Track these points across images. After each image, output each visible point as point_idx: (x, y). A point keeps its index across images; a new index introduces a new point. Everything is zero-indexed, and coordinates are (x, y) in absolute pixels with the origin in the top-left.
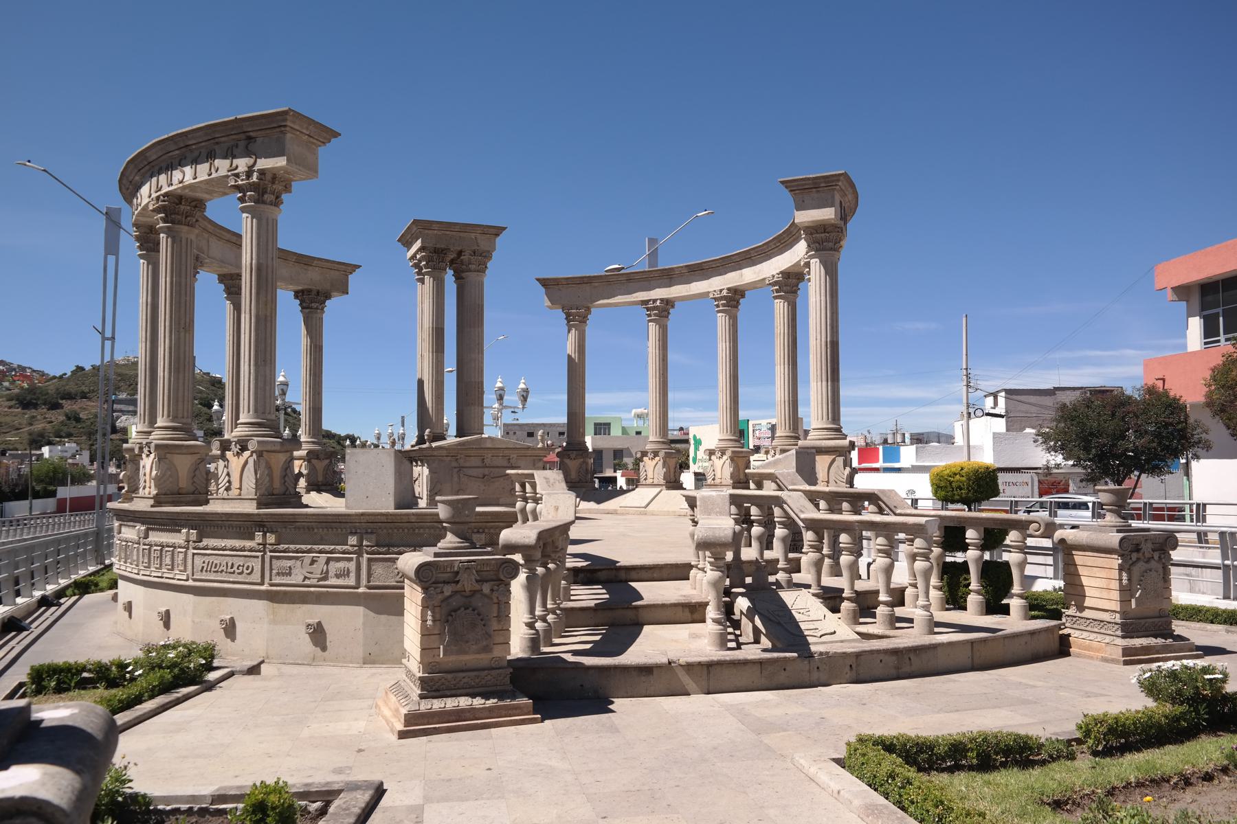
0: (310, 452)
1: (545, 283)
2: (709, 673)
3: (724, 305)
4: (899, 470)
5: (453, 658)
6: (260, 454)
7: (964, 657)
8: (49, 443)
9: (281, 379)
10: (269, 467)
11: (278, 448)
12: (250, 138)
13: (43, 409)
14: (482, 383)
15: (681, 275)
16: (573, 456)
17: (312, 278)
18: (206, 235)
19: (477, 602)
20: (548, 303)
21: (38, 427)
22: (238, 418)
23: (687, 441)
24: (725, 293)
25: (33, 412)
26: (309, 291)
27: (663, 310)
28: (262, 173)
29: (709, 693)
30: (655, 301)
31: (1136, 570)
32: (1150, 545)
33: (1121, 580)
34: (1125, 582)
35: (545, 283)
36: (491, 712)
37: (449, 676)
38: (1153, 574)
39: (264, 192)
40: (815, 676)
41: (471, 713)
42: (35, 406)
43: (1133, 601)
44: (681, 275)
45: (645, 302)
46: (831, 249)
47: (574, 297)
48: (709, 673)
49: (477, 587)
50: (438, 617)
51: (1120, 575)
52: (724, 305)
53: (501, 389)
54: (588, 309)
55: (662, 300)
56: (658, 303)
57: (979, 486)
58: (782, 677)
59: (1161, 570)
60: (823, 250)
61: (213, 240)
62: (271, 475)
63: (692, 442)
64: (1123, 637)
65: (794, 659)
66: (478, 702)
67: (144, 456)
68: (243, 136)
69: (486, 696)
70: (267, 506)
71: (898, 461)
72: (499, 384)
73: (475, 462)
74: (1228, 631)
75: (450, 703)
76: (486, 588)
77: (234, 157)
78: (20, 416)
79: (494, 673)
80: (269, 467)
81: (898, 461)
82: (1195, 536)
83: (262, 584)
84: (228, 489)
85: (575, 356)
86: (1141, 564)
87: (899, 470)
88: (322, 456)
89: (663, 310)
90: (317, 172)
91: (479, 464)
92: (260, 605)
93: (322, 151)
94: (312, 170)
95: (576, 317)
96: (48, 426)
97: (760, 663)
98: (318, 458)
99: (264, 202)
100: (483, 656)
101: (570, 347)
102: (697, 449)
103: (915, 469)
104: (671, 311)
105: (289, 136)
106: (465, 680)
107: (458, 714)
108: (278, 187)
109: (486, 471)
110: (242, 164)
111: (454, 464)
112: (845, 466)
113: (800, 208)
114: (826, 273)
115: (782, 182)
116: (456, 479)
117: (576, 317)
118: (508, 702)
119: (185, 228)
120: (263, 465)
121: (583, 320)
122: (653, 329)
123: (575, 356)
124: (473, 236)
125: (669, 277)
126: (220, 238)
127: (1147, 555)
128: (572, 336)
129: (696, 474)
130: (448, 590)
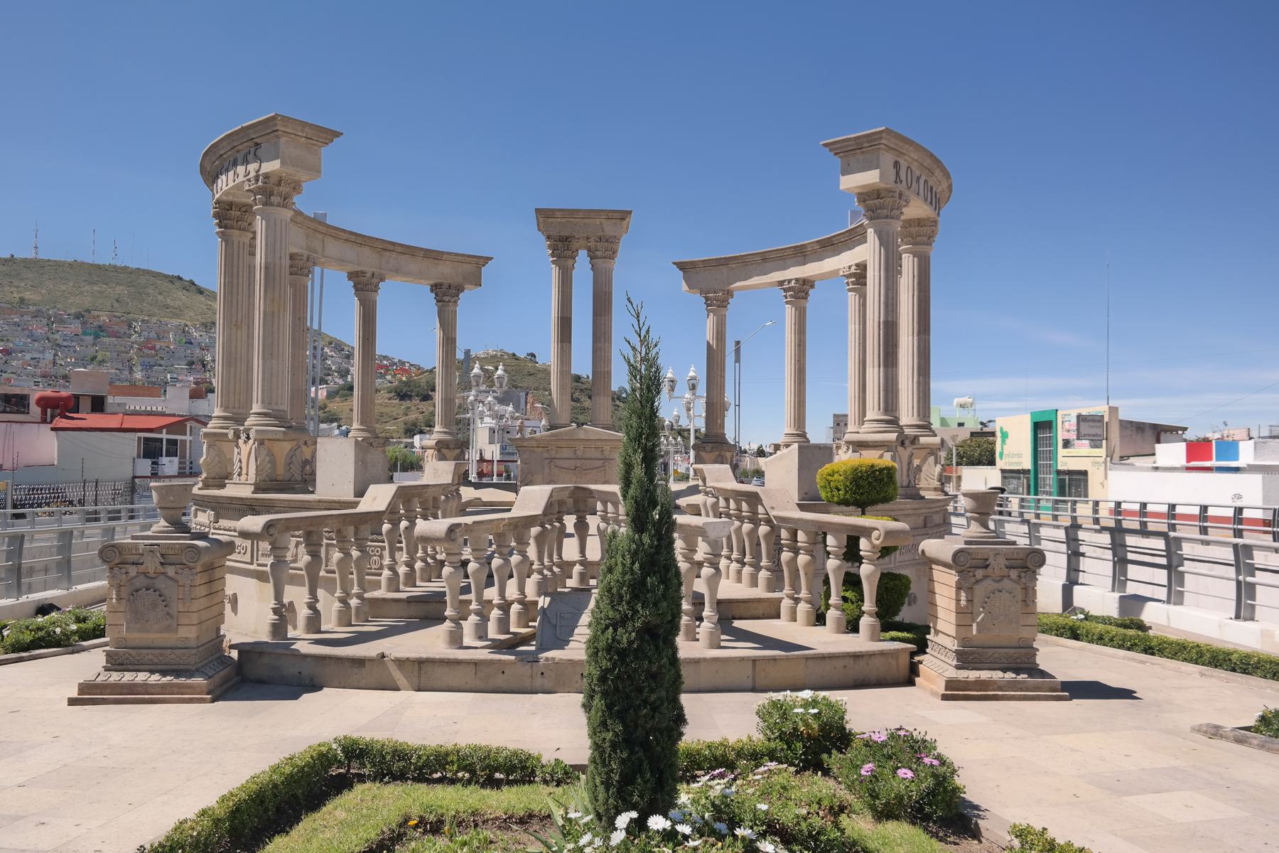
0: (439, 442)
1: (681, 266)
2: (420, 669)
3: (853, 283)
4: (1237, 470)
5: (136, 635)
6: (261, 443)
7: (745, 674)
8: (421, 432)
9: (669, 375)
10: (271, 454)
11: (280, 436)
12: (257, 144)
13: (416, 401)
14: (609, 373)
15: (814, 252)
16: (708, 449)
17: (445, 271)
18: (320, 236)
19: (161, 583)
20: (685, 287)
21: (412, 416)
22: (864, 415)
23: (993, 434)
24: (853, 270)
25: (407, 403)
26: (441, 285)
27: (801, 290)
28: (267, 176)
29: (419, 690)
30: (790, 281)
31: (980, 590)
32: (1002, 561)
33: (958, 600)
34: (963, 603)
35: (681, 266)
36: (163, 688)
37: (133, 652)
38: (1005, 595)
39: (271, 194)
40: (539, 682)
41: (145, 688)
42: (410, 397)
43: (974, 625)
44: (814, 252)
45: (781, 283)
46: (887, 217)
47: (712, 280)
48: (420, 669)
49: (161, 569)
50: (124, 595)
51: (958, 594)
52: (853, 283)
53: (693, 378)
54: (730, 294)
55: (797, 280)
56: (793, 284)
57: (858, 486)
58: (500, 681)
59: (1019, 595)
60: (878, 218)
61: (328, 240)
62: (273, 462)
63: (998, 434)
64: (958, 668)
65: (511, 663)
66: (155, 678)
67: (241, 442)
68: (250, 143)
69: (164, 673)
70: (265, 491)
71: (1237, 459)
72: (692, 374)
73: (566, 453)
74: (1202, 675)
75: (128, 677)
76: (171, 571)
77: (248, 163)
78: (398, 407)
79: (176, 651)
80: (271, 454)
81: (1237, 459)
82: (1229, 554)
83: (252, 563)
84: (240, 475)
85: (714, 343)
86: (989, 581)
87: (1237, 470)
88: (452, 446)
89: (801, 290)
90: (319, 172)
91: (571, 455)
92: (253, 582)
93: (325, 150)
94: (315, 170)
95: (718, 301)
96: (420, 416)
97: (476, 664)
98: (448, 448)
99: (272, 205)
100: (166, 635)
101: (709, 335)
102: (1003, 442)
103: (1252, 469)
104: (811, 292)
105: (283, 140)
106: (150, 657)
107: (131, 688)
108: (284, 189)
109: (578, 463)
110: (252, 167)
111: (546, 455)
112: (936, 463)
113: (845, 172)
114: (881, 245)
115: (825, 145)
116: (547, 471)
117: (718, 301)
118: (182, 680)
119: (236, 232)
120: (264, 452)
121: (723, 304)
122: (789, 311)
123: (714, 343)
124: (598, 222)
125: (801, 254)
126: (337, 238)
127: (998, 572)
128: (710, 323)
129: (1003, 471)
130: (133, 571)
